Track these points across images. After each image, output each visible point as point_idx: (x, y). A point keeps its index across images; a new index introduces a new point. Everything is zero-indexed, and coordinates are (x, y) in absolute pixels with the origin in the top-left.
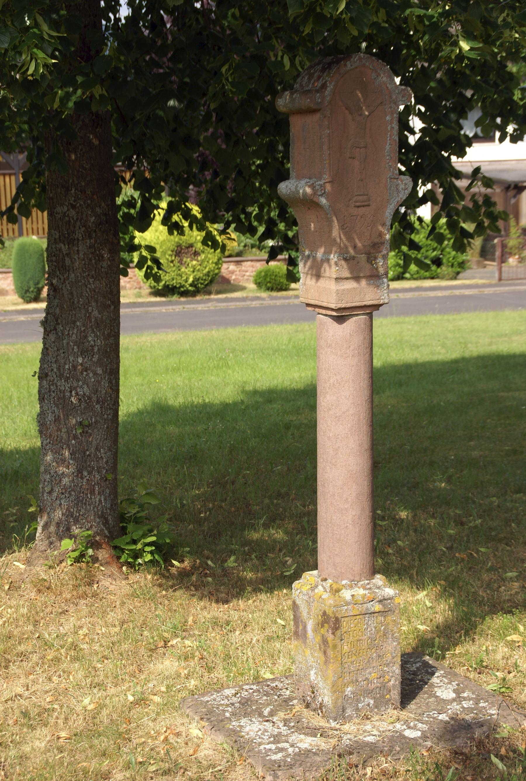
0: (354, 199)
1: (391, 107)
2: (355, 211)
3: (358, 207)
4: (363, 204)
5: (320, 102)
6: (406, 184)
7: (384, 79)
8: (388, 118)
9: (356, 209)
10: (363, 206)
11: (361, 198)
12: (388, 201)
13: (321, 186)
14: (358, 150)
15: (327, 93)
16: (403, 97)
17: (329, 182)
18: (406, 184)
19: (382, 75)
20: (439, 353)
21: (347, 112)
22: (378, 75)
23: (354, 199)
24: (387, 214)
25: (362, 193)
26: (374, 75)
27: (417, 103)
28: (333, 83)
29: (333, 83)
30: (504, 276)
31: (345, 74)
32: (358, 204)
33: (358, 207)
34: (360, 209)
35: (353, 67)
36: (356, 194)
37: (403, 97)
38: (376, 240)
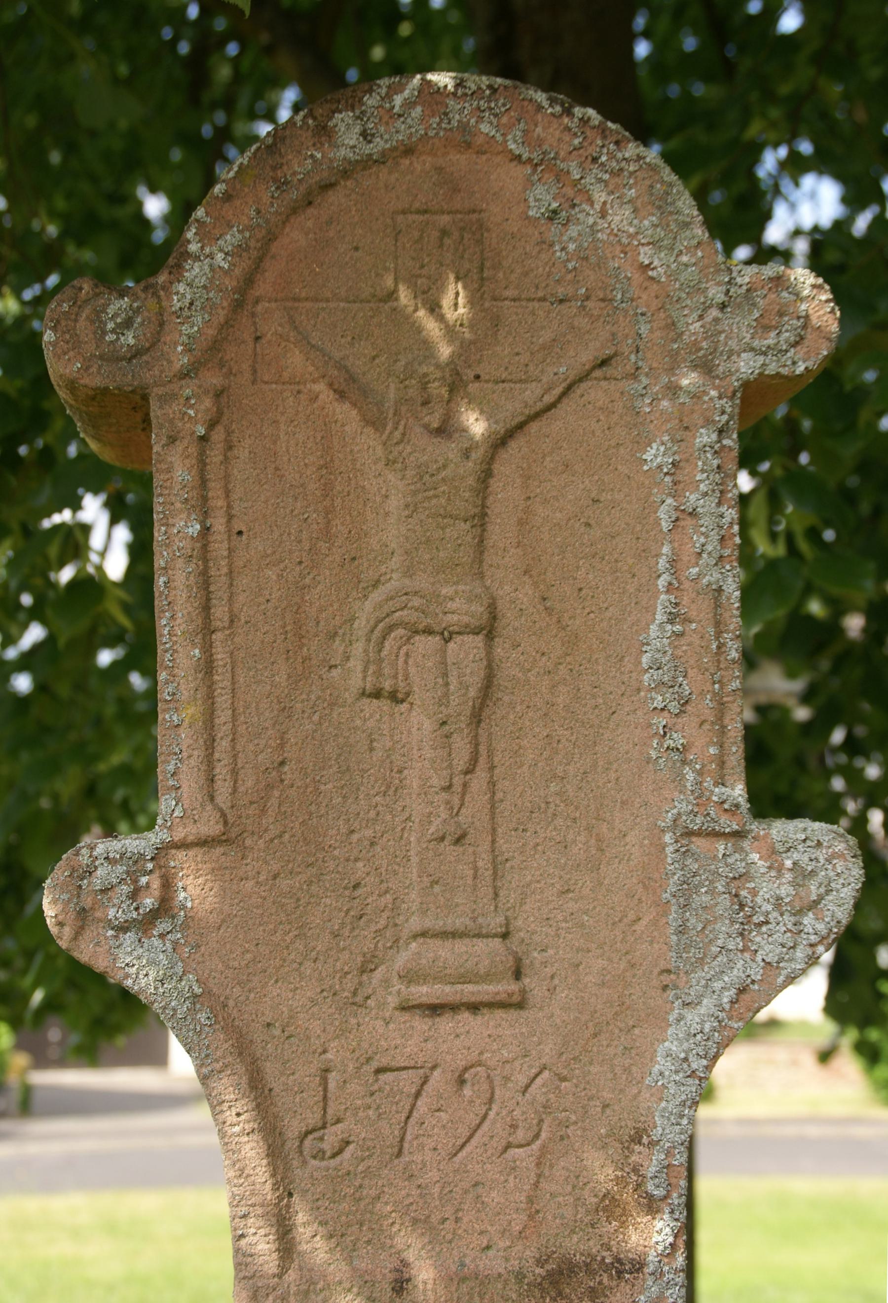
0: (402, 959)
1: (673, 390)
2: (411, 1039)
3: (435, 1009)
4: (470, 991)
5: (137, 353)
6: (802, 875)
7: (620, 218)
8: (655, 455)
9: (420, 1024)
10: (474, 1008)
11: (447, 953)
12: (668, 980)
13: (135, 865)
14: (425, 644)
15: (181, 293)
16: (763, 327)
17: (203, 843)
18: (802, 875)
19: (600, 196)
20: (215, 1082)
21: (346, 415)
22: (575, 197)
23: (402, 959)
24: (662, 1064)
25: (459, 922)
26: (542, 197)
27: (270, 116)
28: (231, 239)
29: (231, 239)
30: (699, 844)
31: (327, 187)
32: (424, 992)
33: (435, 1009)
34: (446, 1024)
35: (379, 145)
36: (415, 923)
37: (763, 327)
38: (576, 1246)
